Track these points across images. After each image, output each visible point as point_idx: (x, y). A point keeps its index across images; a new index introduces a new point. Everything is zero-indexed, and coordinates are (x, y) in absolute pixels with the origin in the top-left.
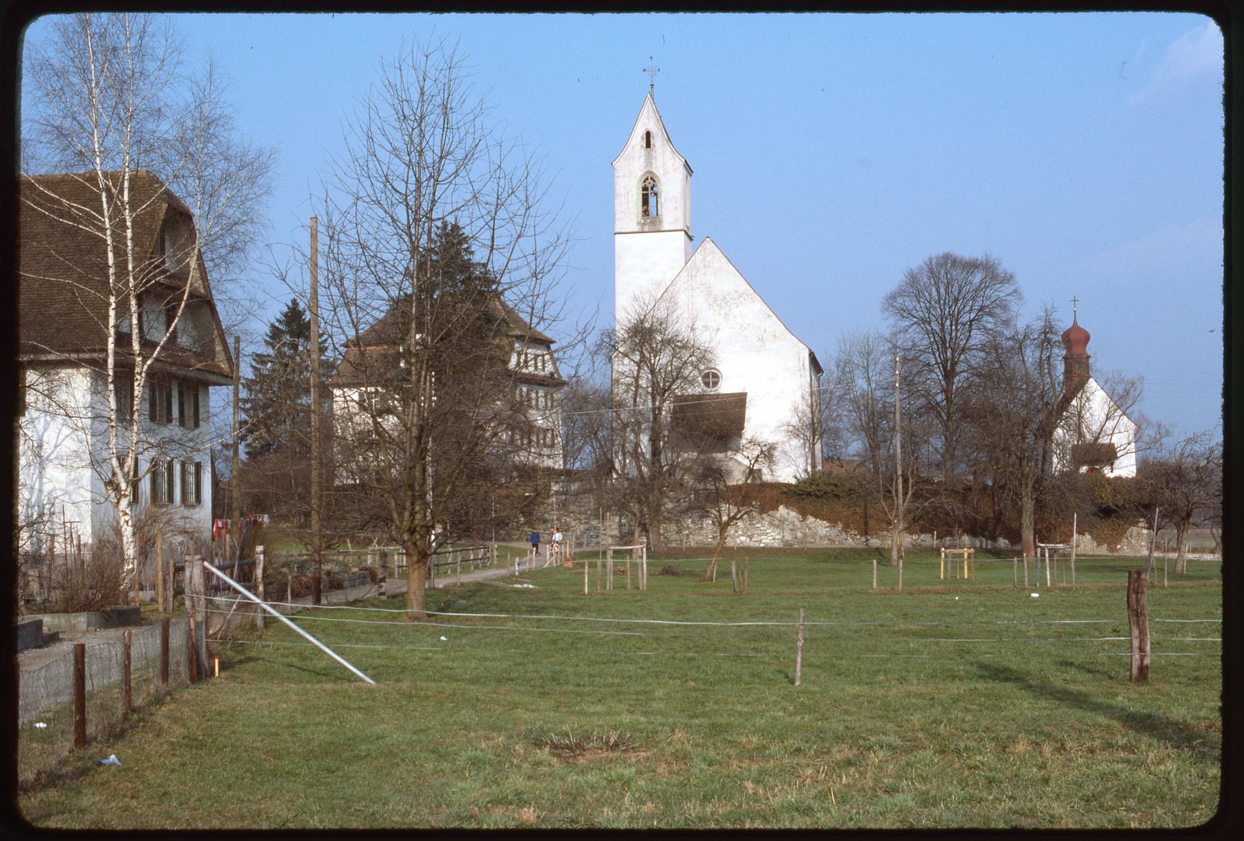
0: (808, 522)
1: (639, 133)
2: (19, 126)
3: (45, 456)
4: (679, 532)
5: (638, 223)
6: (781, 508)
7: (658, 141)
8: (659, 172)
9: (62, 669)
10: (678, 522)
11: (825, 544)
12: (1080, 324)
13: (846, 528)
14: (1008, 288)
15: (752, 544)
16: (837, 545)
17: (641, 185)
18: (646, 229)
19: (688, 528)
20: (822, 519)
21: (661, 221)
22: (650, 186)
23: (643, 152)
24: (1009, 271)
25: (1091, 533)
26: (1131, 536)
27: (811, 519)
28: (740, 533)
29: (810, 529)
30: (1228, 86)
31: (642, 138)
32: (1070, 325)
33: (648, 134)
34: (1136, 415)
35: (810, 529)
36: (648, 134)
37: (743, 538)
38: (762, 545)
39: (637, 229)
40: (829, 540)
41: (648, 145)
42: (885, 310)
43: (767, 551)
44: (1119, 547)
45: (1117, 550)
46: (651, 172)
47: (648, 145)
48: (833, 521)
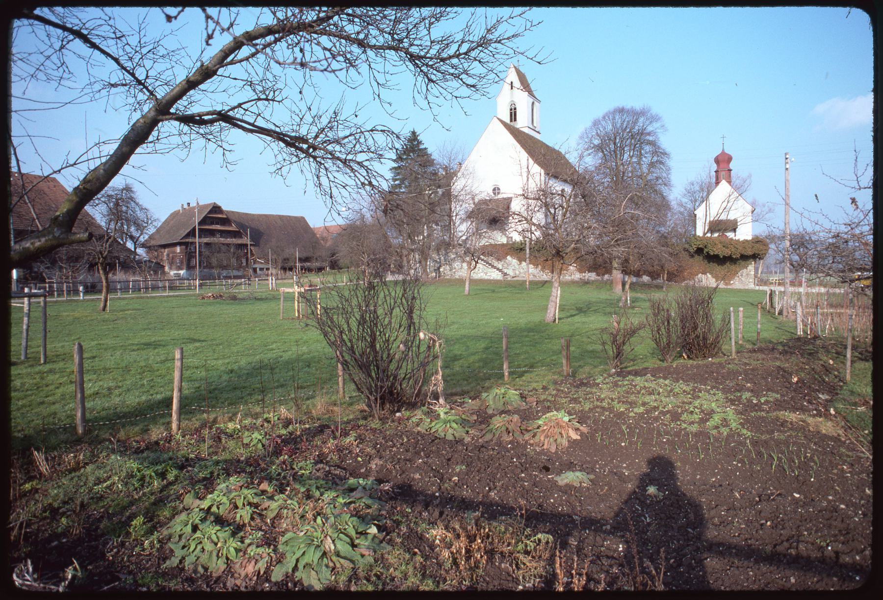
4: (451, 270)
6: (509, 257)
9: (867, 228)
10: (450, 265)
12: (726, 151)
13: (543, 269)
14: (656, 125)
16: (538, 279)
24: (660, 116)
25: (711, 274)
26: (742, 275)
30: (876, 130)
32: (720, 152)
34: (750, 200)
37: (482, 274)
40: (533, 275)
41: (817, 199)
44: (732, 282)
45: (731, 284)
47: (817, 199)
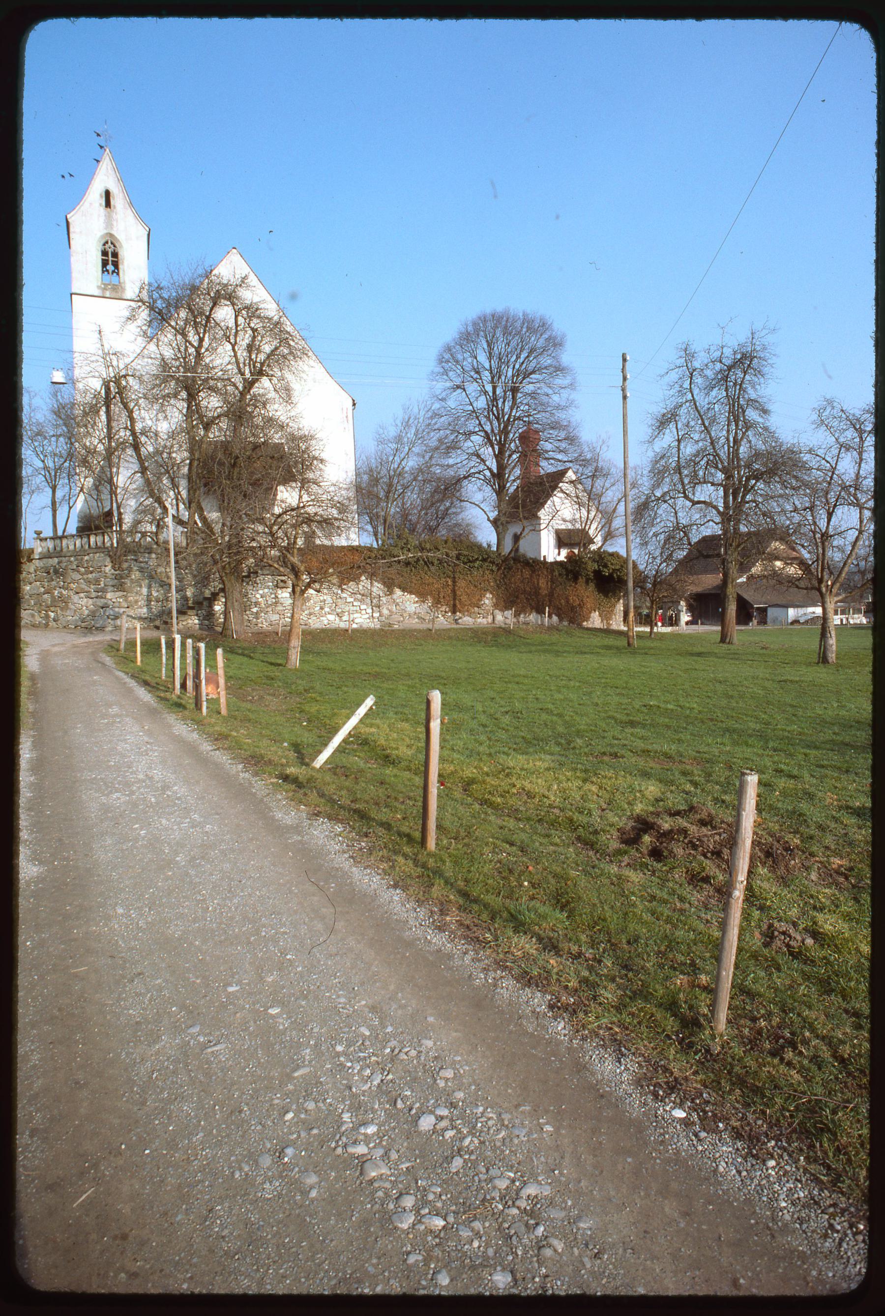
0: (395, 596)
1: (94, 195)
2: (16, 1022)
3: (659, 794)
5: (99, 287)
7: (118, 200)
8: (120, 236)
11: (414, 623)
15: (343, 625)
17: (100, 248)
18: (108, 294)
19: (257, 604)
20: (411, 593)
21: (123, 290)
22: (110, 251)
23: (102, 210)
27: (398, 592)
28: (327, 610)
29: (397, 604)
31: (101, 196)
33: (108, 194)
35: (397, 604)
36: (108, 194)
37: (331, 617)
38: (355, 626)
39: (97, 292)
40: (418, 618)
41: (108, 204)
42: (564, 336)
43: (362, 633)
46: (111, 235)
47: (108, 204)
48: (422, 596)
